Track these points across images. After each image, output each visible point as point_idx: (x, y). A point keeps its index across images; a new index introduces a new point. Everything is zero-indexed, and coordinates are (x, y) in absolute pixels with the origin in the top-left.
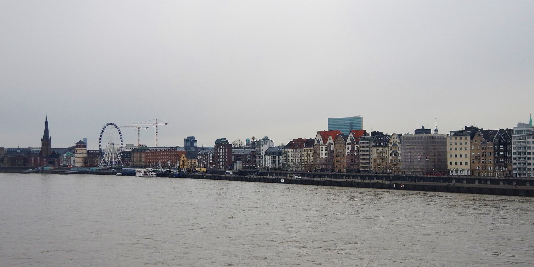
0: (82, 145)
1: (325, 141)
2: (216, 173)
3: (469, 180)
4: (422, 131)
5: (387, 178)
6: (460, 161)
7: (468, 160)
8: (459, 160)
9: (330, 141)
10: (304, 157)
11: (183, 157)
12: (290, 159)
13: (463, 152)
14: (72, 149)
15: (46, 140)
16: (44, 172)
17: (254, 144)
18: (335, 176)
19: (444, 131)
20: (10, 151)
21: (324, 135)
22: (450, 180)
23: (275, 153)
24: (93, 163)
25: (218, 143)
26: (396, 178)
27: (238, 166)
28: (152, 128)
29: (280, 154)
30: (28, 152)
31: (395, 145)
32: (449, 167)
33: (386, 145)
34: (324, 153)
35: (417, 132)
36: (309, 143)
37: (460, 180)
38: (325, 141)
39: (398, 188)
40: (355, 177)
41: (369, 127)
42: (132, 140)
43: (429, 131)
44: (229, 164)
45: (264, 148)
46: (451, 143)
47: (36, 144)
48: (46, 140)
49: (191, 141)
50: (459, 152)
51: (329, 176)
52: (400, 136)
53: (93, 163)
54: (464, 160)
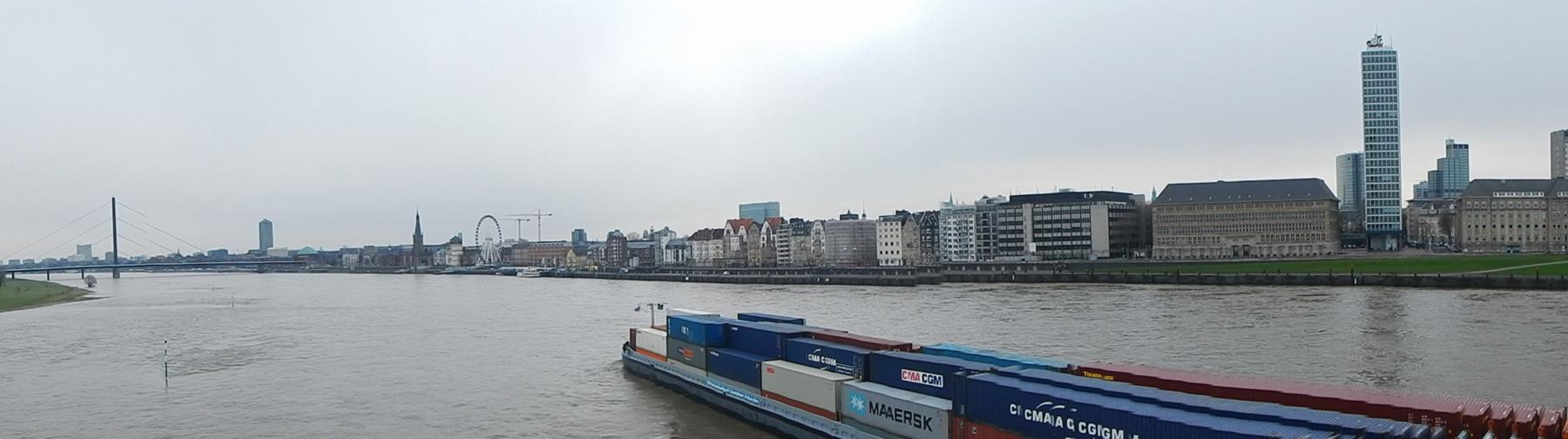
0: (457, 241)
1: (736, 231)
2: (611, 272)
3: (903, 271)
4: (849, 216)
5: (808, 271)
6: (892, 248)
7: (900, 248)
8: (889, 248)
9: (742, 231)
10: (712, 250)
11: (571, 254)
12: (696, 252)
13: (894, 240)
14: (446, 246)
15: (418, 236)
16: (416, 272)
17: (653, 236)
18: (749, 272)
19: (872, 216)
20: (381, 250)
21: (735, 224)
22: (880, 271)
23: (677, 246)
24: (470, 262)
25: (611, 236)
26: (820, 271)
27: (635, 262)
28: (534, 220)
29: (684, 247)
30: (399, 249)
31: (818, 233)
32: (879, 256)
33: (808, 234)
34: (735, 245)
35: (842, 217)
36: (718, 234)
37: (890, 271)
38: (736, 231)
39: (822, 282)
40: (773, 272)
41: (787, 214)
42: (511, 234)
43: (856, 217)
44: (625, 259)
45: (665, 241)
46: (881, 228)
47: (1320, 156)
48: (418, 236)
49: (579, 234)
50: (889, 240)
51: (742, 272)
52: (823, 222)
53: (470, 262)
54: (895, 248)
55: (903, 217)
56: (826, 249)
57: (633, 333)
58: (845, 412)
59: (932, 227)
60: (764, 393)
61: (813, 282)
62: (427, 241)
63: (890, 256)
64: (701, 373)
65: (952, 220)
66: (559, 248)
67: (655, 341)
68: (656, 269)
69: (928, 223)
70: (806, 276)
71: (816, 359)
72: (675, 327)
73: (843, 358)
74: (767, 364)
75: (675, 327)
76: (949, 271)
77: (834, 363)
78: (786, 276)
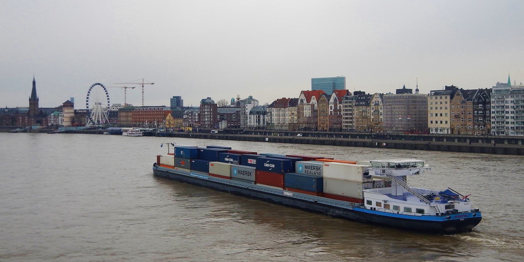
0: (69, 104)
1: (308, 101)
3: (450, 138)
5: (369, 136)
7: (448, 119)
8: (439, 119)
9: (314, 100)
11: (169, 117)
12: (274, 118)
13: (443, 111)
14: (59, 109)
15: (34, 99)
16: (31, 131)
17: (239, 104)
18: (318, 135)
19: (424, 91)
21: (307, 95)
22: (430, 138)
24: (81, 123)
25: (204, 103)
26: (378, 137)
27: (223, 125)
28: (139, 88)
29: (265, 113)
31: (377, 104)
32: (430, 125)
33: (368, 105)
34: (307, 112)
35: (398, 91)
36: (293, 102)
37: (440, 138)
38: (308, 101)
39: (380, 146)
41: (351, 87)
42: (118, 100)
43: (410, 91)
44: (215, 123)
45: (249, 108)
46: (432, 102)
48: (34, 99)
49: (177, 101)
50: (439, 112)
52: (381, 95)
53: (81, 123)
55: (452, 91)
56: (382, 116)
57: (159, 158)
58: (232, 176)
59: (485, 103)
60: (210, 174)
61: (372, 146)
62: (42, 104)
63: (439, 126)
64: (188, 171)
65: (510, 99)
66: (158, 113)
67: (169, 160)
68: (241, 131)
69: (481, 98)
70: (366, 140)
71: (227, 159)
72: (179, 152)
73: (234, 158)
74: (211, 163)
75: (179, 152)
76: (506, 145)
77: (232, 160)
78: (349, 139)
